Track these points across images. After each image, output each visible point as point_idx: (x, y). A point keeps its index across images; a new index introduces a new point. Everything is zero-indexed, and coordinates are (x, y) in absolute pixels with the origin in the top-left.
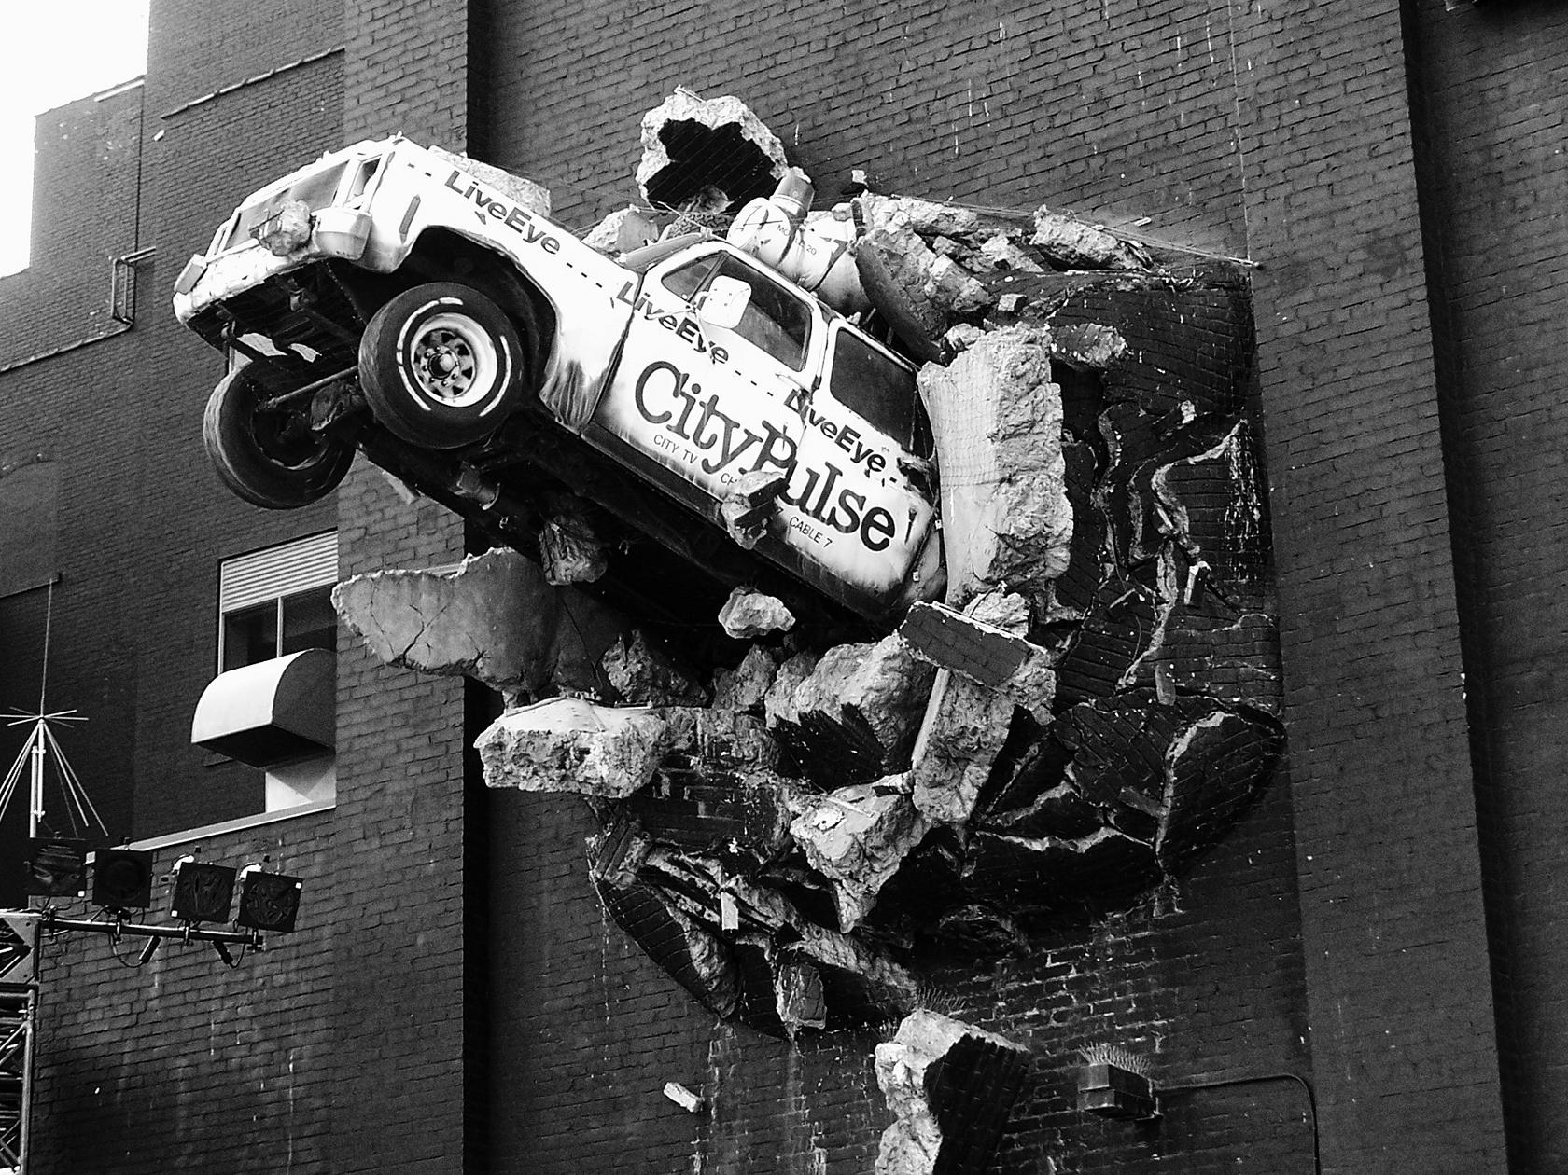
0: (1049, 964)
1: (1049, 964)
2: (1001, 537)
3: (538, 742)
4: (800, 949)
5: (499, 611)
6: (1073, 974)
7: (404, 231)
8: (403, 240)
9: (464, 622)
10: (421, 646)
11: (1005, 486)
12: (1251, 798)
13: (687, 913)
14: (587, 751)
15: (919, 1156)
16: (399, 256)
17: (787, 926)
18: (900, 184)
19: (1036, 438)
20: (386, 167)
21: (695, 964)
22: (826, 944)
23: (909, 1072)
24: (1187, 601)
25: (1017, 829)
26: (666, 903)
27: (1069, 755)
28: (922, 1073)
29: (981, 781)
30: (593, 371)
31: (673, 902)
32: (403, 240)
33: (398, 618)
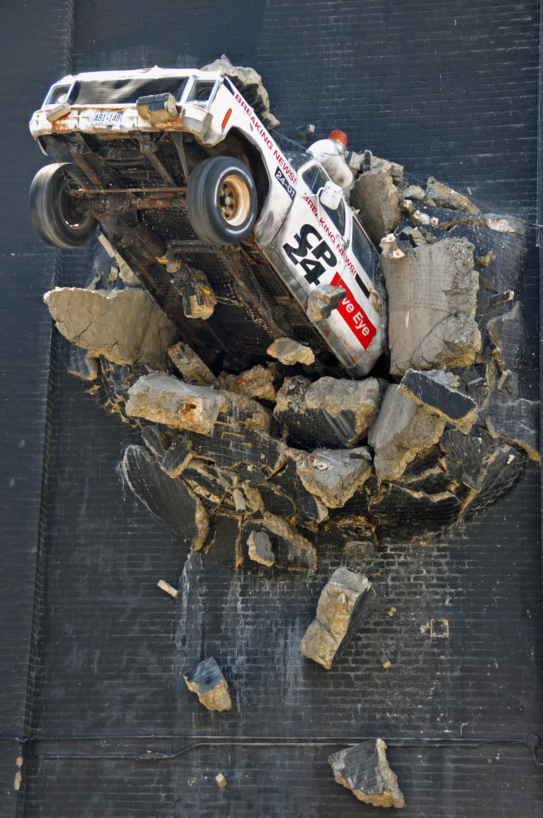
0: (388, 552)
1: (388, 552)
2: (447, 343)
3: (168, 398)
4: (261, 524)
5: (128, 321)
6: (402, 559)
7: (223, 126)
8: (223, 131)
9: (112, 324)
10: (89, 332)
11: (453, 319)
12: (510, 489)
13: (198, 495)
14: (194, 407)
15: (331, 640)
16: (219, 139)
17: (259, 511)
18: (268, 128)
19: (468, 297)
20: (219, 88)
21: (196, 522)
22: (274, 523)
23: (347, 599)
24: (499, 387)
25: (409, 486)
26: (188, 489)
27: (443, 455)
28: (355, 600)
29: (410, 461)
30: (278, 218)
31: (192, 489)
32: (223, 131)
33: (80, 315)
